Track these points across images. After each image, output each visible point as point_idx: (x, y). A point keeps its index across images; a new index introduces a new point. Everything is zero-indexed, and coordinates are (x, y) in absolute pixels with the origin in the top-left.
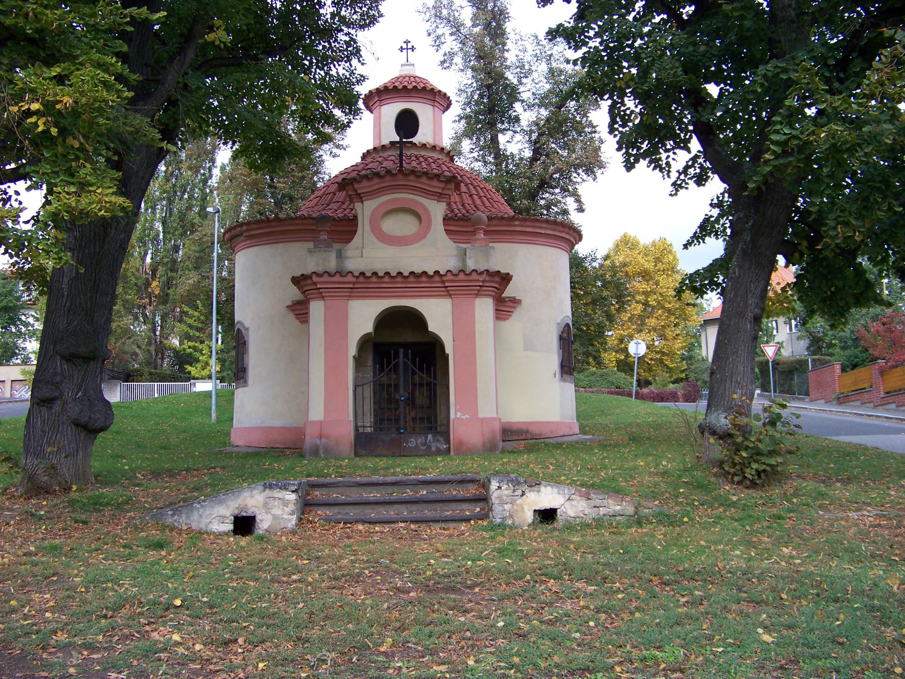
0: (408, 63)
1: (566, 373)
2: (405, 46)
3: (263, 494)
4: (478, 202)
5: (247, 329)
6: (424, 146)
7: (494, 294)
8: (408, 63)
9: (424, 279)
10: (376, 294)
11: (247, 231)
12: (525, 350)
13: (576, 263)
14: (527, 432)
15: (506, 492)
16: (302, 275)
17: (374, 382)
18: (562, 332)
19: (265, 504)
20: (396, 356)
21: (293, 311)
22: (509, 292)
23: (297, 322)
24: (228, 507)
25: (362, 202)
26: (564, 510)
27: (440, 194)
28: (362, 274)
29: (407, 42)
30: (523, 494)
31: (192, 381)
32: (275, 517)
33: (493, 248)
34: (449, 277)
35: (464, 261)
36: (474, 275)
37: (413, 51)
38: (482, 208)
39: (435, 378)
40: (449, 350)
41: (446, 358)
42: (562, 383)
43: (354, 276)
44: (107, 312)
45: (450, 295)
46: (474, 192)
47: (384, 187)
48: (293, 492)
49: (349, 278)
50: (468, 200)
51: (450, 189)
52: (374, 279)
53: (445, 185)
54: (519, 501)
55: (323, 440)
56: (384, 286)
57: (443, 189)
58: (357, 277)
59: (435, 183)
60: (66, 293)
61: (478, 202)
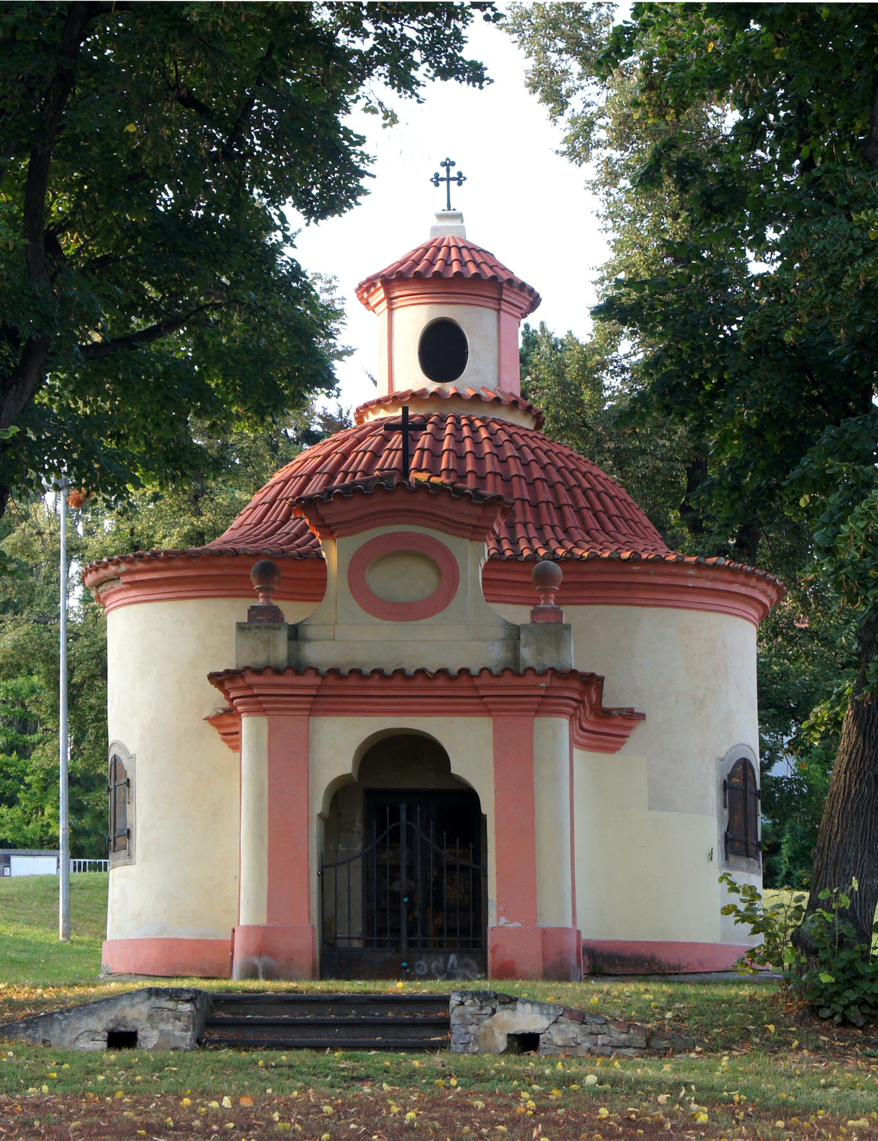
0: (450, 214)
1: (737, 853)
3: (147, 1003)
5: (132, 758)
8: (450, 214)
9: (441, 682)
11: (127, 573)
12: (650, 809)
14: (652, 960)
15: (471, 1009)
18: (730, 776)
19: (150, 1017)
20: (395, 817)
21: (218, 727)
24: (100, 1019)
26: (549, 1036)
27: (474, 526)
29: (448, 164)
30: (494, 1011)
32: (162, 1033)
34: (486, 680)
35: (515, 651)
37: (460, 184)
38: (578, 535)
40: (488, 806)
41: (480, 820)
48: (187, 1001)
49: (310, 680)
54: (487, 1022)
56: (372, 693)
57: (479, 519)
58: (323, 677)
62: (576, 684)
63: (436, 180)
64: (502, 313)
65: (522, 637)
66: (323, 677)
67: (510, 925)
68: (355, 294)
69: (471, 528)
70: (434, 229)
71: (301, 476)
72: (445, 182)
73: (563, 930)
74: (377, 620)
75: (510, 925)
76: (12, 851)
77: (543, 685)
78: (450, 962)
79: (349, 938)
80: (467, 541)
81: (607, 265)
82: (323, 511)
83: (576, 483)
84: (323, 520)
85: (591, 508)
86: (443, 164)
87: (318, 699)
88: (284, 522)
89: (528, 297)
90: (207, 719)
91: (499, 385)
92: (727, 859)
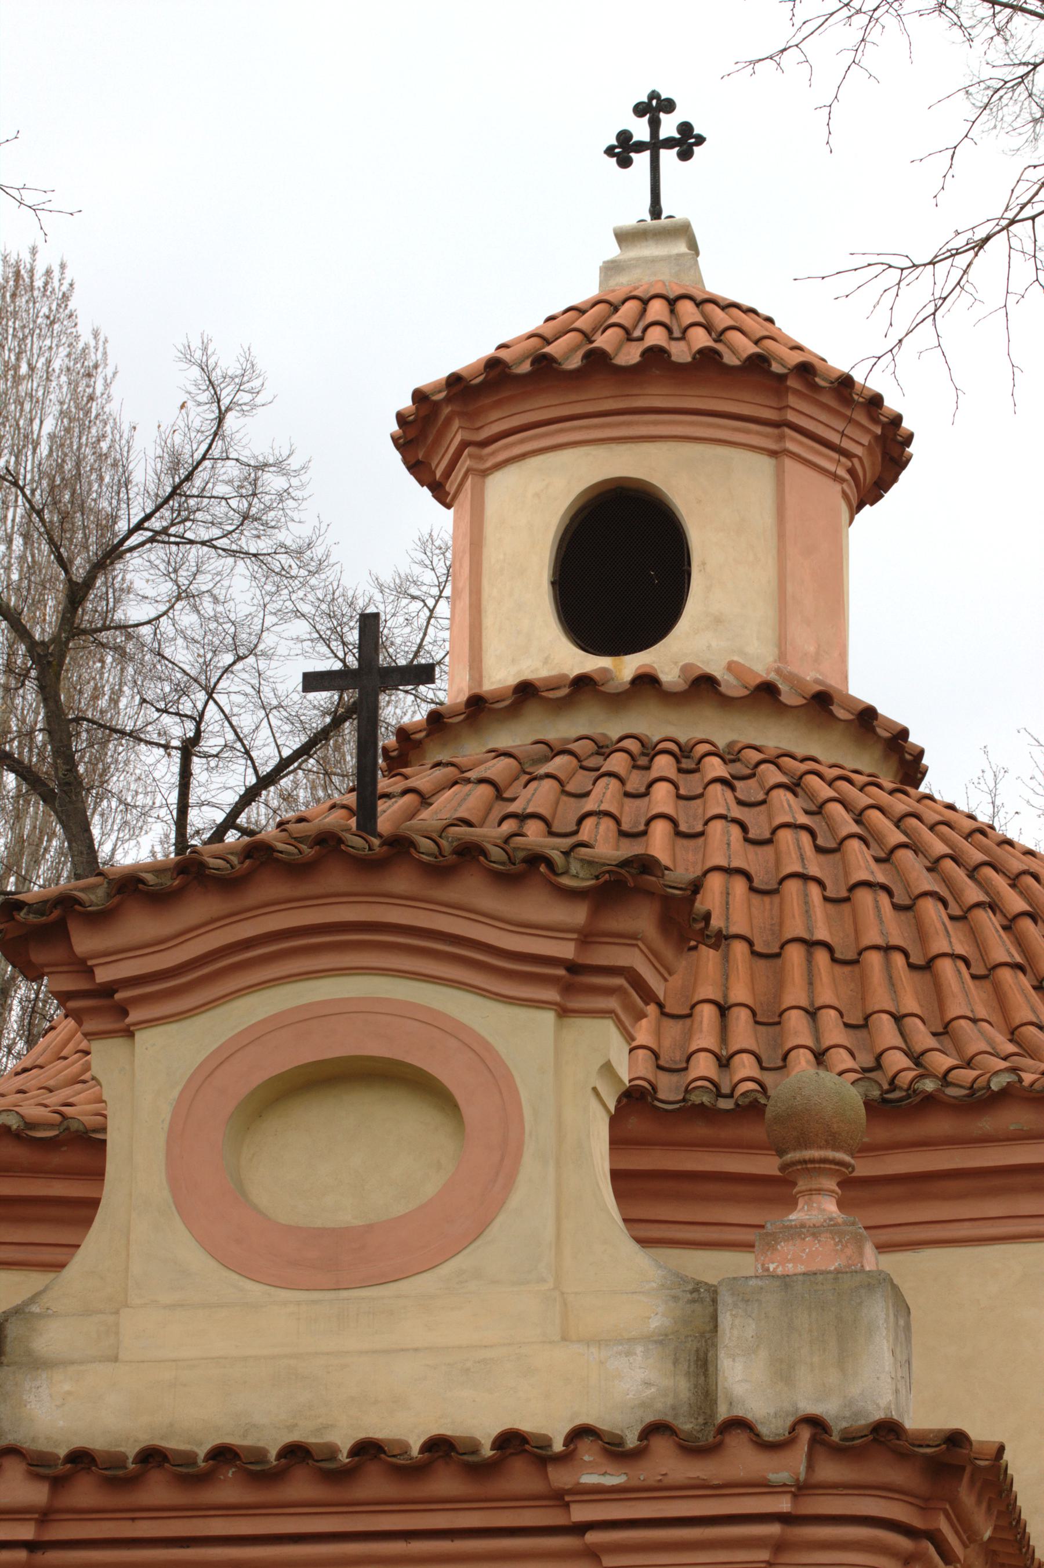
2: (641, 131)
27: (573, 968)
36: (739, 1448)
37: (685, 155)
51: (630, 939)
53: (595, 912)
57: (586, 938)
66: (58, 1483)
68: (397, 456)
69: (561, 972)
70: (610, 268)
83: (982, 897)
84: (90, 972)
86: (640, 110)
89: (865, 421)
91: (782, 656)
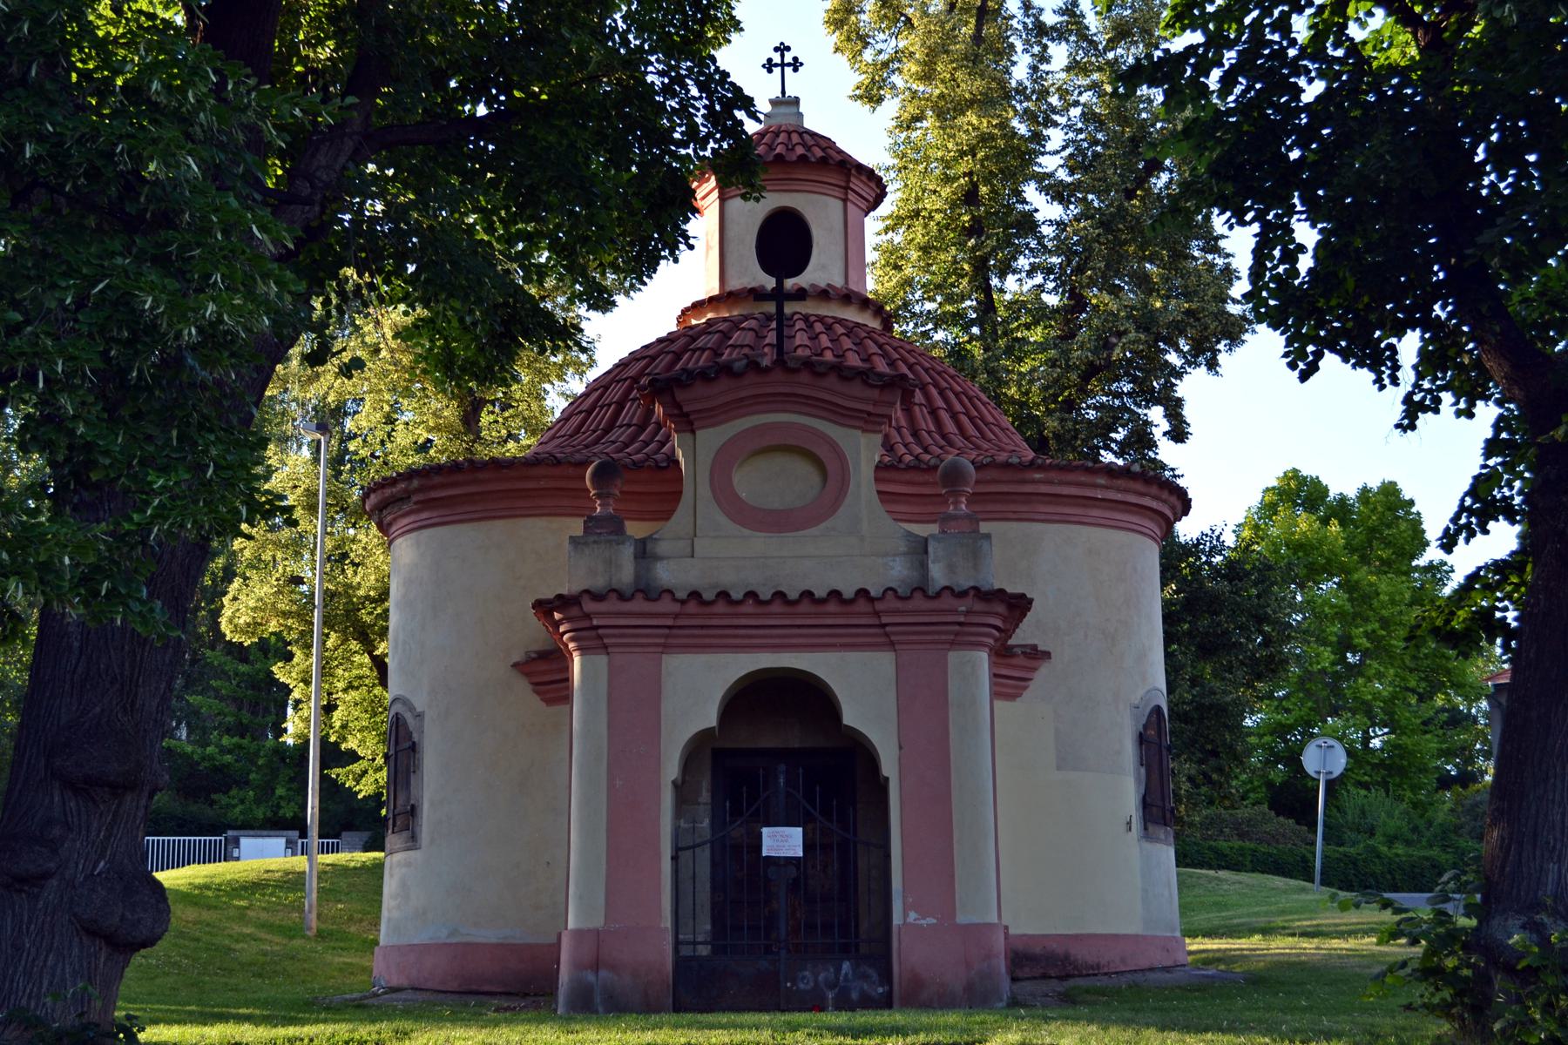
1: (1156, 823)
2: (777, 58)
4: (950, 427)
5: (419, 716)
6: (824, 294)
7: (991, 641)
10: (707, 641)
13: (1175, 557)
16: (560, 597)
17: (712, 843)
18: (1145, 727)
21: (527, 674)
22: (1025, 634)
23: (535, 701)
25: (693, 432)
28: (695, 595)
29: (782, 49)
31: (230, 833)
33: (988, 536)
35: (924, 566)
36: (947, 597)
37: (796, 70)
38: (959, 441)
39: (855, 834)
40: (889, 767)
41: (882, 786)
42: (1147, 846)
43: (675, 600)
44: (163, 686)
45: (892, 644)
46: (940, 403)
47: (742, 400)
49: (666, 605)
50: (925, 422)
52: (721, 608)
55: (603, 973)
56: (744, 622)
58: (683, 602)
59: (856, 389)
60: (76, 644)
61: (950, 427)
62: (1001, 608)
63: (769, 66)
64: (849, 204)
65: (930, 549)
67: (922, 922)
71: (626, 379)
72: (779, 69)
73: (990, 926)
74: (747, 532)
75: (922, 922)
76: (242, 832)
77: (963, 608)
78: (843, 972)
79: (695, 943)
80: (859, 433)
81: (890, 216)
82: (680, 395)
85: (967, 414)
87: (675, 631)
88: (606, 431)
90: (515, 665)
92: (1146, 829)
